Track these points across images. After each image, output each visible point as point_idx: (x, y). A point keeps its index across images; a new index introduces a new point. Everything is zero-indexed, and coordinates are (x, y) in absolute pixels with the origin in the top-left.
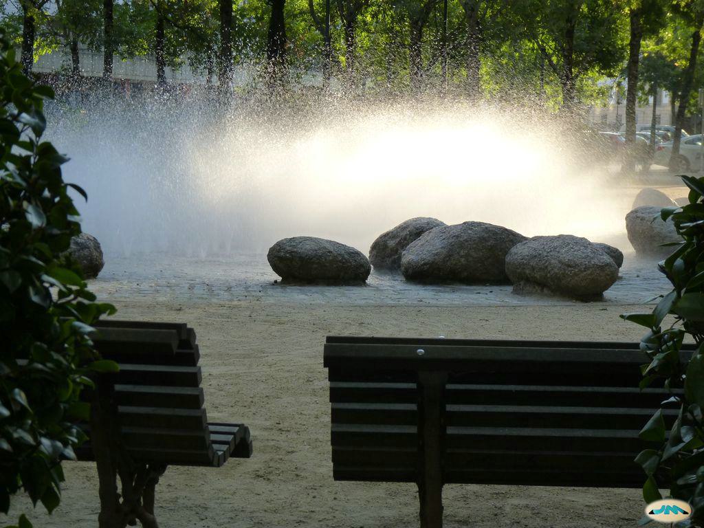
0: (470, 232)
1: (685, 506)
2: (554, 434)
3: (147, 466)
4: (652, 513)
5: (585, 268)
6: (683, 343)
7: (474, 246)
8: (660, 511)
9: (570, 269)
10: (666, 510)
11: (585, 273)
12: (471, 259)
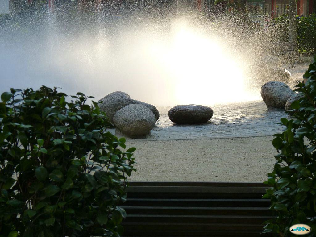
0: (110, 101)
1: (307, 227)
2: (193, 201)
3: (292, 177)
4: (293, 230)
5: (132, 122)
6: (304, 137)
7: (111, 109)
8: (296, 229)
9: (126, 122)
10: (299, 229)
11: (132, 124)
12: (109, 115)
